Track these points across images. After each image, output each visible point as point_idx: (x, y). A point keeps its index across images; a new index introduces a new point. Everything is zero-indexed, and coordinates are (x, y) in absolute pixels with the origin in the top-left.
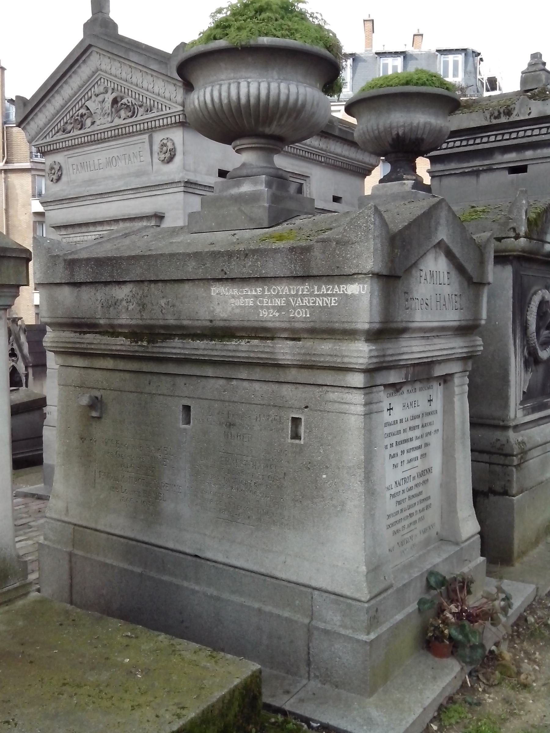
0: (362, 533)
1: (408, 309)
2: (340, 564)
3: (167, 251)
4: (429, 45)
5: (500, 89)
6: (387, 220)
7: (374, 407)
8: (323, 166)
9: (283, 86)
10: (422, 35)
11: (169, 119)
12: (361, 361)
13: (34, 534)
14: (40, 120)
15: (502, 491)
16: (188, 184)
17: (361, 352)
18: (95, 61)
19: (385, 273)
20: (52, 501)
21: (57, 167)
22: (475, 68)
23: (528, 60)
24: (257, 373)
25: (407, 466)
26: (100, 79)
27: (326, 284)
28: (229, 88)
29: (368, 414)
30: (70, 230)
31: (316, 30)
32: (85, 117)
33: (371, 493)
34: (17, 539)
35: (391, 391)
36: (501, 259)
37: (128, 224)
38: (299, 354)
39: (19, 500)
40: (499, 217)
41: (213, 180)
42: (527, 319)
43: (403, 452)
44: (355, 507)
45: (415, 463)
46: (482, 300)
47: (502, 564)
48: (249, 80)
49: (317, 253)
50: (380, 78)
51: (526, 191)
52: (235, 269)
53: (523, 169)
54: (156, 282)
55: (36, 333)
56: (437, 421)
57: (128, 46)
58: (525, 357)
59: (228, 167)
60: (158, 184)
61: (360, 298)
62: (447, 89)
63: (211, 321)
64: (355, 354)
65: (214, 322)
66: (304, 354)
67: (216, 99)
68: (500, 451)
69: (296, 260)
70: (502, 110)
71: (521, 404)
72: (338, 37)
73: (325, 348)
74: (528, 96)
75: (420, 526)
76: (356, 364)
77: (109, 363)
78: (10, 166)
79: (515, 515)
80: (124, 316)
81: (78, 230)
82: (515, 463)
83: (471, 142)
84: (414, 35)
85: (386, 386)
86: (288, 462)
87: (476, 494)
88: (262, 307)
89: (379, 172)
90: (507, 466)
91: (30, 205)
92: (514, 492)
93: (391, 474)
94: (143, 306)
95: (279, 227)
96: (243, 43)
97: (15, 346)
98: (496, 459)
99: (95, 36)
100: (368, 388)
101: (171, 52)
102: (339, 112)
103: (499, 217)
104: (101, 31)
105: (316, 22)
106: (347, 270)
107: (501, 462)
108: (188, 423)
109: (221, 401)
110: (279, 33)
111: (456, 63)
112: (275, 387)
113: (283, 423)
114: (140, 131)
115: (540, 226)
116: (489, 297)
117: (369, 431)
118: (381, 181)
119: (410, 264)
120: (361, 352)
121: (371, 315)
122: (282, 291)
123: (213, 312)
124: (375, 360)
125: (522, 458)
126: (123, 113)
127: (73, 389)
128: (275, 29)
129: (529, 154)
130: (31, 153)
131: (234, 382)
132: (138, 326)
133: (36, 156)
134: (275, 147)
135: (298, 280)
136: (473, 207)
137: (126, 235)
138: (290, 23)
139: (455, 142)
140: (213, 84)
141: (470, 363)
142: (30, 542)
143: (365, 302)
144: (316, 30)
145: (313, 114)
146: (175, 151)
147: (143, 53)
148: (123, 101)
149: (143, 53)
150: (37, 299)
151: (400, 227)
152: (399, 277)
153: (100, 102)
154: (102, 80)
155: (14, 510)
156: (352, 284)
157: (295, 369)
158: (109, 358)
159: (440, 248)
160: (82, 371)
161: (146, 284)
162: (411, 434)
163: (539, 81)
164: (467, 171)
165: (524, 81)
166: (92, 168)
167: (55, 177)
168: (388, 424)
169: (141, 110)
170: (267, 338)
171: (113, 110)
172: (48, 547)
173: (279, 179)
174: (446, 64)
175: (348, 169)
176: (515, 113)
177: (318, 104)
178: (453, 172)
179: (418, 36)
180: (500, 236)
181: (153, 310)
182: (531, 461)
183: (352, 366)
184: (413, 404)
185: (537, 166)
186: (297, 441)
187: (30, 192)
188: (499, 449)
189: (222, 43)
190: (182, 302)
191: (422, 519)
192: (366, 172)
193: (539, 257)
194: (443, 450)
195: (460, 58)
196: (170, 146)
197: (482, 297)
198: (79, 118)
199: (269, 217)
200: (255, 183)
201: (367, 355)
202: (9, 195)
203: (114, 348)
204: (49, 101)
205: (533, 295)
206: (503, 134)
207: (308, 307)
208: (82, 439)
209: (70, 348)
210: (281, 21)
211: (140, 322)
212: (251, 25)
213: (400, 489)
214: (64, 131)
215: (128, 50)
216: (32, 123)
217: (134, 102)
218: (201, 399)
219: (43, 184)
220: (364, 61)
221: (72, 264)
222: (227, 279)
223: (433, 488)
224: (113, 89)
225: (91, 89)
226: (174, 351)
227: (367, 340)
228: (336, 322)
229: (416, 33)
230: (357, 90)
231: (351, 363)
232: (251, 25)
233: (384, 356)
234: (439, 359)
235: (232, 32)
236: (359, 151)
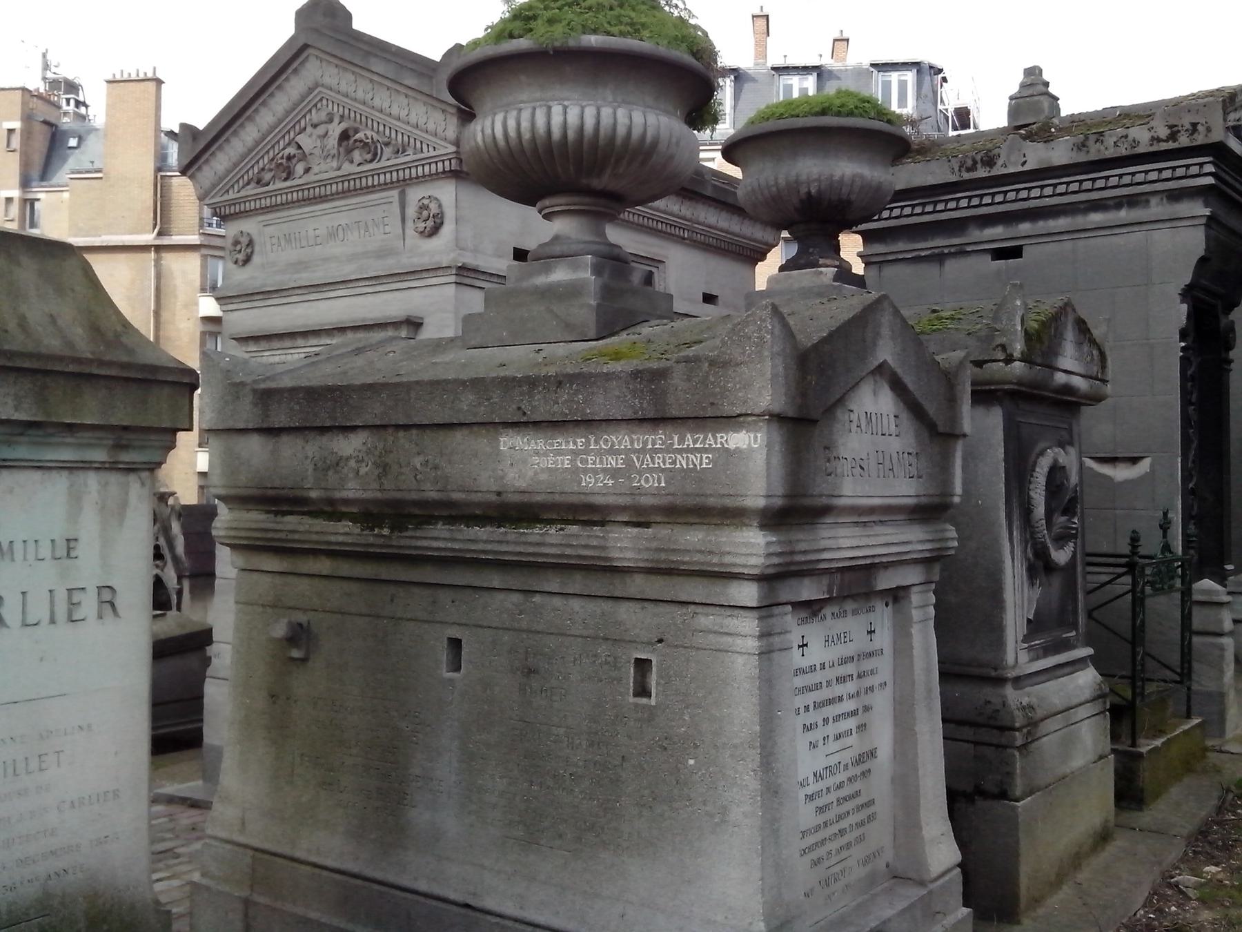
0: (758, 861)
1: (830, 475)
2: (720, 918)
3: (426, 377)
4: (859, 55)
5: (975, 127)
6: (793, 328)
7: (776, 640)
8: (688, 245)
9: (621, 113)
10: (848, 40)
11: (433, 166)
12: (753, 561)
13: (184, 868)
14: (221, 162)
15: (996, 790)
16: (463, 270)
17: (751, 546)
18: (314, 70)
19: (790, 414)
20: (217, 807)
21: (244, 240)
22: (935, 93)
23: (1020, 77)
24: (577, 583)
25: (833, 746)
26: (321, 100)
27: (693, 431)
28: (533, 115)
29: (765, 654)
30: (264, 345)
31: (675, 26)
32: (294, 161)
33: (772, 790)
34: (155, 876)
35: (804, 615)
36: (984, 396)
37: (361, 335)
38: (647, 549)
39: (159, 808)
40: (978, 326)
41: (503, 264)
42: (1030, 498)
43: (826, 721)
44: (745, 815)
45: (849, 741)
46: (954, 463)
47: (1000, 920)
48: (566, 103)
49: (677, 380)
50: (778, 105)
51: (1021, 286)
52: (541, 407)
53: (1016, 252)
54: (406, 427)
55: (198, 520)
56: (884, 668)
57: (366, 47)
58: (1028, 560)
59: (530, 244)
60: (415, 270)
61: (749, 455)
62: (889, 121)
63: (499, 494)
64: (744, 550)
65: (504, 496)
66: (658, 550)
67: (512, 133)
68: (992, 722)
69: (642, 391)
70: (978, 158)
71: (1023, 641)
72: (711, 37)
73: (692, 540)
74: (1021, 135)
75: (857, 852)
76: (745, 566)
77: (324, 566)
78: (166, 241)
79: (1021, 835)
80: (350, 485)
81: (276, 344)
82: (1019, 743)
83: (929, 208)
84: (835, 40)
85: (798, 605)
86: (629, 737)
87: (953, 796)
88: (585, 471)
89: (776, 258)
90: (1005, 747)
91: (197, 304)
92: (1018, 793)
93: (806, 760)
94: (384, 469)
95: (615, 339)
96: (557, 44)
97: (162, 542)
98: (985, 735)
99: (317, 31)
100: (765, 609)
101: (438, 58)
102: (714, 161)
103: (978, 326)
104: (326, 25)
105: (676, 14)
106: (728, 410)
107: (995, 741)
108: (457, 668)
109: (515, 630)
110: (615, 30)
111: (903, 85)
112: (607, 606)
113: (619, 669)
114: (386, 184)
115: (1046, 343)
116: (964, 459)
117: (767, 682)
118: (782, 269)
119: (833, 400)
120: (751, 546)
121: (769, 484)
122: (620, 443)
123: (502, 478)
124: (776, 560)
125: (1029, 733)
126: (357, 156)
127: (261, 609)
128: (609, 23)
129: (1025, 227)
130: (201, 219)
131: (537, 599)
132: (376, 502)
133: (210, 225)
134: (608, 211)
135: (645, 425)
136: (934, 311)
137: (358, 351)
138: (633, 14)
139: (902, 207)
140: (506, 108)
141: (937, 568)
142: (176, 883)
143: (759, 462)
144: (675, 26)
145: (671, 157)
146: (442, 218)
147: (394, 59)
148: (357, 136)
149: (394, 59)
150: (203, 461)
151: (815, 339)
152: (814, 422)
153: (319, 137)
154: (324, 102)
155: (151, 826)
156: (737, 432)
157: (642, 576)
158: (323, 558)
159: (881, 374)
160: (278, 580)
161: (390, 431)
162: (839, 690)
163: (1040, 111)
164: (923, 254)
165: (1014, 112)
166: (304, 243)
167: (241, 257)
168: (800, 672)
169: (388, 151)
170: (594, 523)
171: (342, 150)
172: (208, 888)
173: (614, 263)
174: (887, 86)
175: (728, 251)
176: (1000, 162)
177: (678, 143)
178: (900, 256)
179: (841, 41)
180: (980, 358)
181: (402, 474)
182: (1045, 739)
183: (736, 570)
184: (843, 638)
185: (1040, 247)
186: (644, 701)
187: (198, 284)
188: (990, 718)
189: (523, 44)
190: (450, 462)
191: (860, 839)
192: (758, 255)
193: (1046, 394)
194: (895, 717)
195: (910, 77)
196: (434, 208)
197: (954, 456)
198: (284, 161)
199: (598, 321)
200: (576, 267)
201: (762, 552)
202: (163, 288)
203: (333, 539)
204: (235, 133)
205: (1037, 458)
206: (981, 196)
207: (663, 471)
208: (273, 696)
209: (258, 539)
210: (618, 11)
211: (379, 495)
212: (571, 16)
213: (821, 785)
214: (258, 182)
215: (368, 54)
216: (206, 168)
217: (376, 137)
218: (481, 627)
219: (219, 270)
220: (753, 80)
221: (266, 397)
222: (526, 424)
223: (880, 786)
224: (342, 116)
225: (305, 116)
226: (435, 544)
227: (763, 526)
228: (711, 495)
229: (837, 36)
230: (741, 123)
231: (735, 565)
232: (571, 16)
233: (792, 553)
234: (884, 560)
235: (540, 26)
236: (747, 222)
